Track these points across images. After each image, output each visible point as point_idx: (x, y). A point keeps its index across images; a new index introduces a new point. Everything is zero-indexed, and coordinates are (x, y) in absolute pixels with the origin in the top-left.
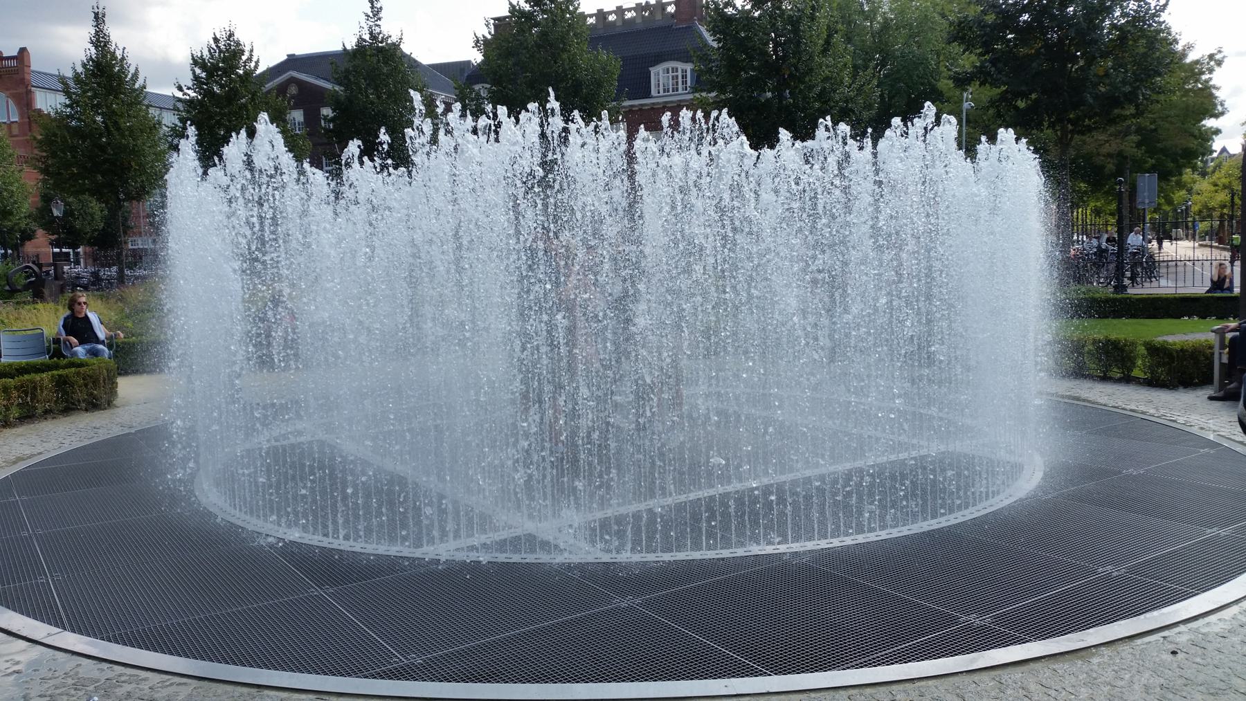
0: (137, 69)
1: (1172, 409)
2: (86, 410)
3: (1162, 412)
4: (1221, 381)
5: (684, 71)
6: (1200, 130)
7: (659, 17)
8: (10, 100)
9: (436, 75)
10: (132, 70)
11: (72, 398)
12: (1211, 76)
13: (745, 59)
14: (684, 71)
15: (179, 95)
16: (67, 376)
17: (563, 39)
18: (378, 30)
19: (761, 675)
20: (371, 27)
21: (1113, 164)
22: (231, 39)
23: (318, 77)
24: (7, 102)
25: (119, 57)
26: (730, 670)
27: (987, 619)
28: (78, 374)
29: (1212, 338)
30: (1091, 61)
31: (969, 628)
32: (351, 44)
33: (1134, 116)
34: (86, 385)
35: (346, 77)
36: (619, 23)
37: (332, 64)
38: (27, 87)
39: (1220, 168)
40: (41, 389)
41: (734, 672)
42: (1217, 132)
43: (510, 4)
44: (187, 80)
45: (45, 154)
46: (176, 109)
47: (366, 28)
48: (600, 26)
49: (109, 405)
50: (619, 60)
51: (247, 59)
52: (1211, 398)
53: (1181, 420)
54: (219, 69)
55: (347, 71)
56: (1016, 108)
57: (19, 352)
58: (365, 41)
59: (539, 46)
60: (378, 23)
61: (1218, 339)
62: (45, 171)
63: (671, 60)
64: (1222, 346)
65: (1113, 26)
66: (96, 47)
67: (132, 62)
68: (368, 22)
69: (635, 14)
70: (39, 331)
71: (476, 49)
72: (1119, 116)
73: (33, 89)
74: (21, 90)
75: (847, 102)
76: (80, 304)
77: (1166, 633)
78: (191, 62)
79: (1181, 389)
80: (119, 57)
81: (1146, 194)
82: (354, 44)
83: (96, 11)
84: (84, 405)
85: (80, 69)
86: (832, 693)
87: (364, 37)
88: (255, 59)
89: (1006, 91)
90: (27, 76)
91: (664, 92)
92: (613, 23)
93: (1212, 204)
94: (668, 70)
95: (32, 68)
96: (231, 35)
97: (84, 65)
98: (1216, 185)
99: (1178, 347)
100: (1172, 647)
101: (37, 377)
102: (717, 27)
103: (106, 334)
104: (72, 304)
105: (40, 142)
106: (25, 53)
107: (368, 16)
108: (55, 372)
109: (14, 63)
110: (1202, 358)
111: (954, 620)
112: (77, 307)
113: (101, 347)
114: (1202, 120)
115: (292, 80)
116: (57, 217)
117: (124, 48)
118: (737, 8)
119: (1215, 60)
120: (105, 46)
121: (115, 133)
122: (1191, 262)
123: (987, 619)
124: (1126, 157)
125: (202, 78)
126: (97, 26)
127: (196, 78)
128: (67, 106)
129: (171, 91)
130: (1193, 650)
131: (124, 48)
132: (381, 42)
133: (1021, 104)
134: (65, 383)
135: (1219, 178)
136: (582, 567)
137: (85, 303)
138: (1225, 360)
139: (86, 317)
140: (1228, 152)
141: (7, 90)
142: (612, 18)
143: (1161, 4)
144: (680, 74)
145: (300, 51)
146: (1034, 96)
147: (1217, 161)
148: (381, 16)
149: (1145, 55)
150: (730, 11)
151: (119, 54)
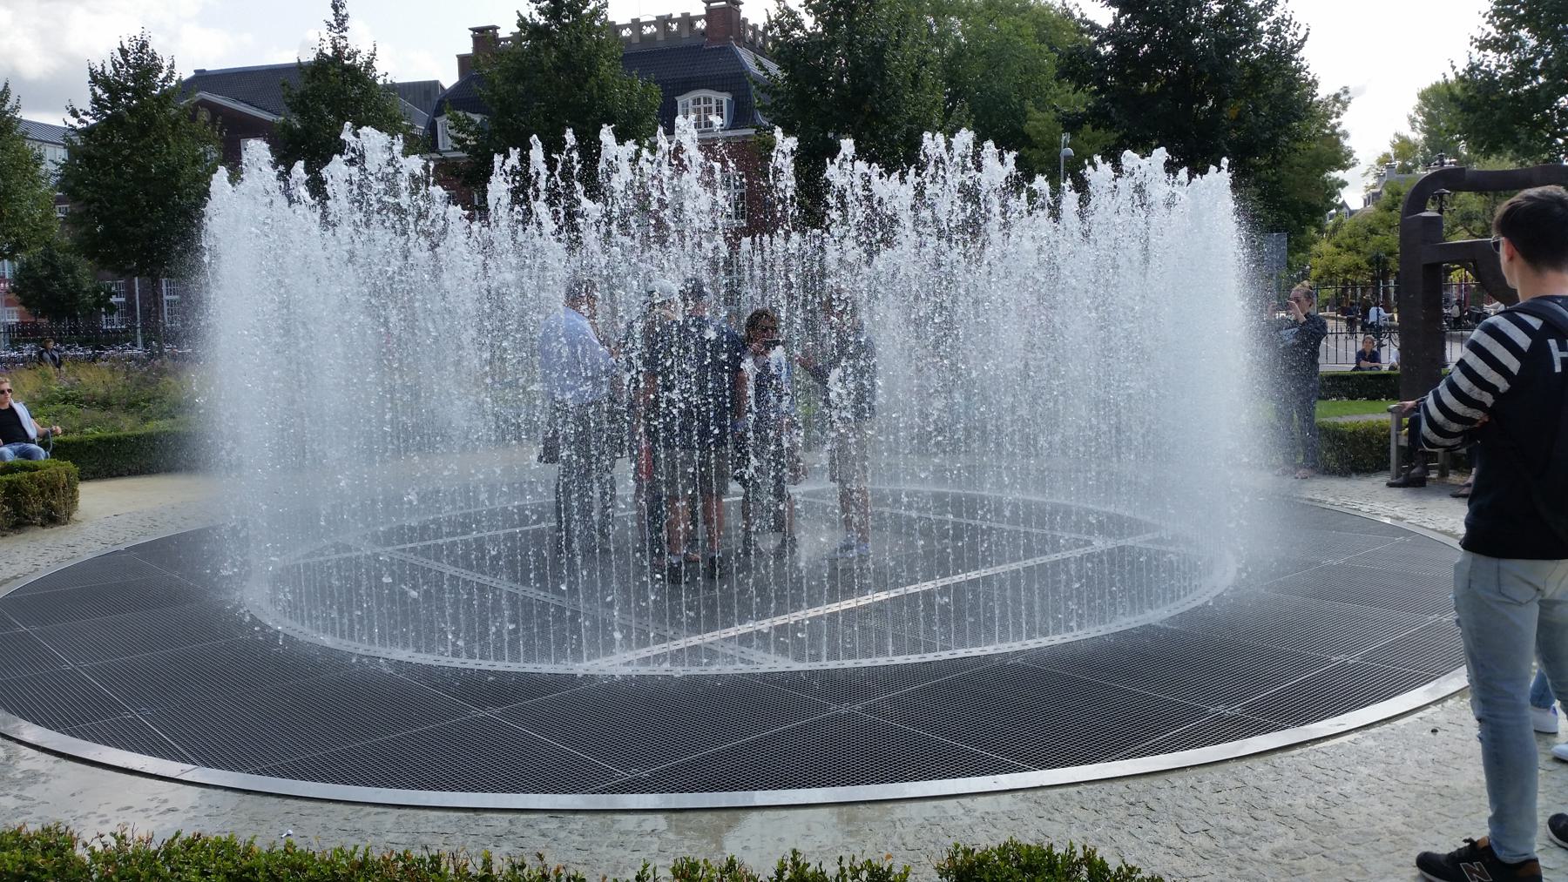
1: (1351, 498)
2: (43, 525)
3: (1342, 500)
4: (1398, 465)
5: (719, 102)
6: (1325, 182)
7: (685, 34)
11: (25, 510)
12: (1339, 120)
13: (816, 92)
14: (719, 102)
15: (74, 121)
16: (19, 483)
17: (591, 60)
18: (343, 43)
20: (334, 39)
22: (144, 51)
23: (238, 100)
27: (1237, 709)
28: (32, 479)
29: (1387, 419)
30: (1221, 101)
31: (1220, 717)
32: (309, 57)
34: (42, 494)
35: (302, 102)
36: (636, 40)
37: (284, 85)
42: (1343, 184)
44: (84, 103)
52: (1390, 485)
53: (1365, 508)
54: (128, 89)
55: (303, 94)
59: (558, 69)
60: (344, 34)
61: (1395, 419)
63: (702, 88)
64: (1400, 427)
68: (330, 33)
69: (655, 30)
77: (1420, 714)
78: (90, 79)
79: (1354, 475)
86: (1108, 784)
87: (325, 51)
91: (706, 126)
92: (628, 39)
93: (1337, 268)
94: (699, 99)
96: (144, 45)
98: (1338, 246)
99: (1350, 429)
100: (1432, 726)
102: (784, 52)
103: (37, 430)
107: (331, 25)
110: (1375, 442)
111: (1204, 712)
113: (34, 446)
114: (1324, 172)
115: (204, 103)
118: (806, 31)
119: (1340, 100)
122: (1334, 336)
123: (1237, 709)
127: (96, 100)
129: (58, 119)
130: (1451, 727)
132: (348, 59)
134: (16, 491)
135: (1343, 239)
136: (765, 676)
137: (10, 391)
138: (1404, 441)
139: (12, 410)
140: (1348, 208)
142: (626, 33)
143: (1299, 39)
144: (714, 105)
145: (211, 66)
147: (1337, 219)
148: (346, 25)
149: (1283, 96)
150: (797, 33)
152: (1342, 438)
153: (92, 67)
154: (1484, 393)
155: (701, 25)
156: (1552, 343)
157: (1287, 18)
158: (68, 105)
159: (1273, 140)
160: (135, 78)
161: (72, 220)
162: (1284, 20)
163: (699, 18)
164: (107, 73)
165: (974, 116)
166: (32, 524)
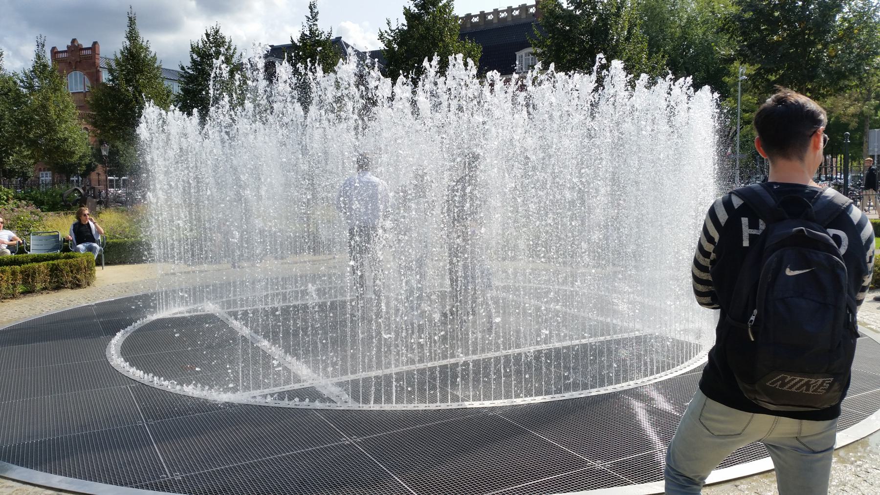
2: (72, 288)
7: (524, 16)
8: (86, 77)
16: (58, 265)
18: (315, 28)
19: (629, 484)
20: (310, 26)
21: (856, 122)
26: (563, 483)
33: (857, 86)
34: (72, 272)
36: (496, 21)
38: (97, 68)
40: (39, 274)
41: (582, 487)
46: (179, 82)
49: (89, 285)
57: (42, 247)
58: (306, 35)
60: (316, 23)
62: (94, 124)
65: (844, 19)
66: (130, 41)
69: (506, 14)
70: (57, 233)
71: (380, 41)
72: (846, 86)
76: (85, 215)
81: (876, 144)
83: (130, 16)
84: (69, 285)
85: (119, 56)
87: (305, 33)
88: (232, 48)
89: (760, 69)
97: (122, 53)
101: (36, 265)
104: (79, 215)
105: (92, 105)
106: (97, 46)
107: (309, 18)
108: (51, 262)
109: (89, 52)
112: (83, 218)
116: (105, 156)
117: (148, 41)
125: (197, 61)
128: (110, 80)
131: (148, 41)
132: (318, 36)
134: (57, 269)
139: (88, 224)
141: (85, 70)
142: (490, 17)
146: (781, 72)
156: (745, 221)
159: (858, 66)
163: (531, 6)
164: (200, 47)
165: (376, 60)
166: (66, 288)
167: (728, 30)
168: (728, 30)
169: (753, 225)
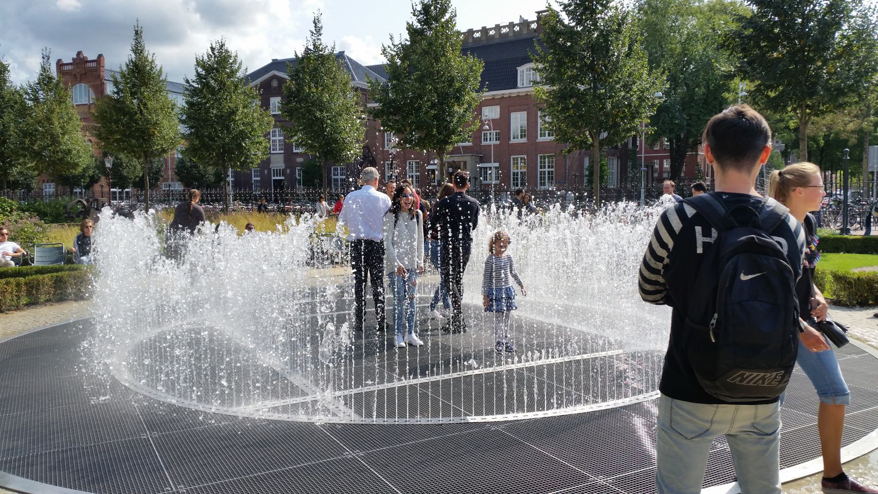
0: (161, 68)
7: (525, 32)
8: (90, 89)
9: (371, 72)
10: (158, 68)
16: (62, 276)
18: (319, 42)
20: (314, 40)
24: (89, 90)
25: (150, 60)
28: (69, 276)
36: (497, 36)
39: (121, 209)
40: (43, 286)
43: (408, 23)
44: (192, 76)
45: (99, 125)
47: (311, 41)
48: (484, 39)
50: (482, 62)
51: (234, 61)
56: (768, 97)
58: (310, 50)
60: (320, 37)
65: (843, 37)
66: (135, 53)
67: (158, 63)
69: (508, 30)
71: (383, 55)
73: (105, 82)
74: (98, 82)
75: (643, 92)
79: (858, 307)
80: (150, 60)
81: (875, 161)
82: (303, 52)
83: (136, 29)
85: (125, 68)
87: (309, 47)
88: (239, 61)
89: (760, 85)
90: (102, 73)
92: (493, 36)
95: (106, 68)
96: (222, 46)
97: (127, 66)
99: (855, 277)
101: (40, 277)
105: (96, 117)
106: (102, 58)
107: (312, 33)
108: (55, 274)
109: (94, 64)
112: (86, 230)
115: (275, 77)
116: (109, 168)
120: (141, 52)
121: (145, 111)
124: (866, 133)
126: (136, 39)
127: (198, 75)
128: (115, 93)
132: (321, 51)
133: (772, 94)
141: (89, 82)
142: (492, 33)
146: (781, 88)
151: (150, 58)
152: (850, 283)
153: (198, 57)
154: (657, 263)
155: (534, 26)
156: (698, 229)
157: (873, 7)
158: (184, 77)
160: (217, 63)
161: (657, 142)
162: (870, 8)
163: (533, 22)
167: (728, 46)
168: (728, 46)
169: (706, 233)
